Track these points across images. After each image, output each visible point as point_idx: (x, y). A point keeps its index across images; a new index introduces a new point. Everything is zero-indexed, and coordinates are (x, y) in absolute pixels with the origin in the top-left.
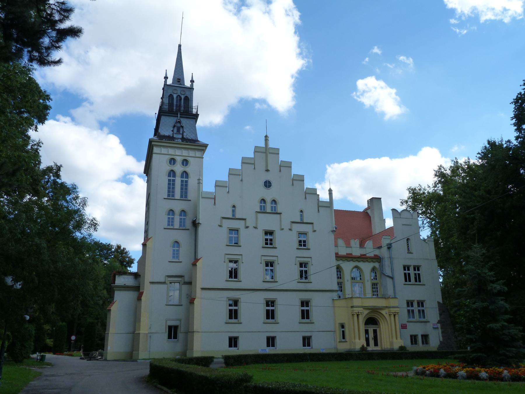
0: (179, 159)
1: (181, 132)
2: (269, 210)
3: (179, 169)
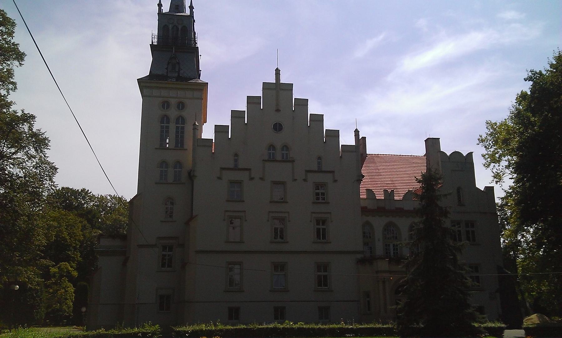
0: (173, 102)
1: (177, 70)
2: (279, 158)
3: (173, 113)
